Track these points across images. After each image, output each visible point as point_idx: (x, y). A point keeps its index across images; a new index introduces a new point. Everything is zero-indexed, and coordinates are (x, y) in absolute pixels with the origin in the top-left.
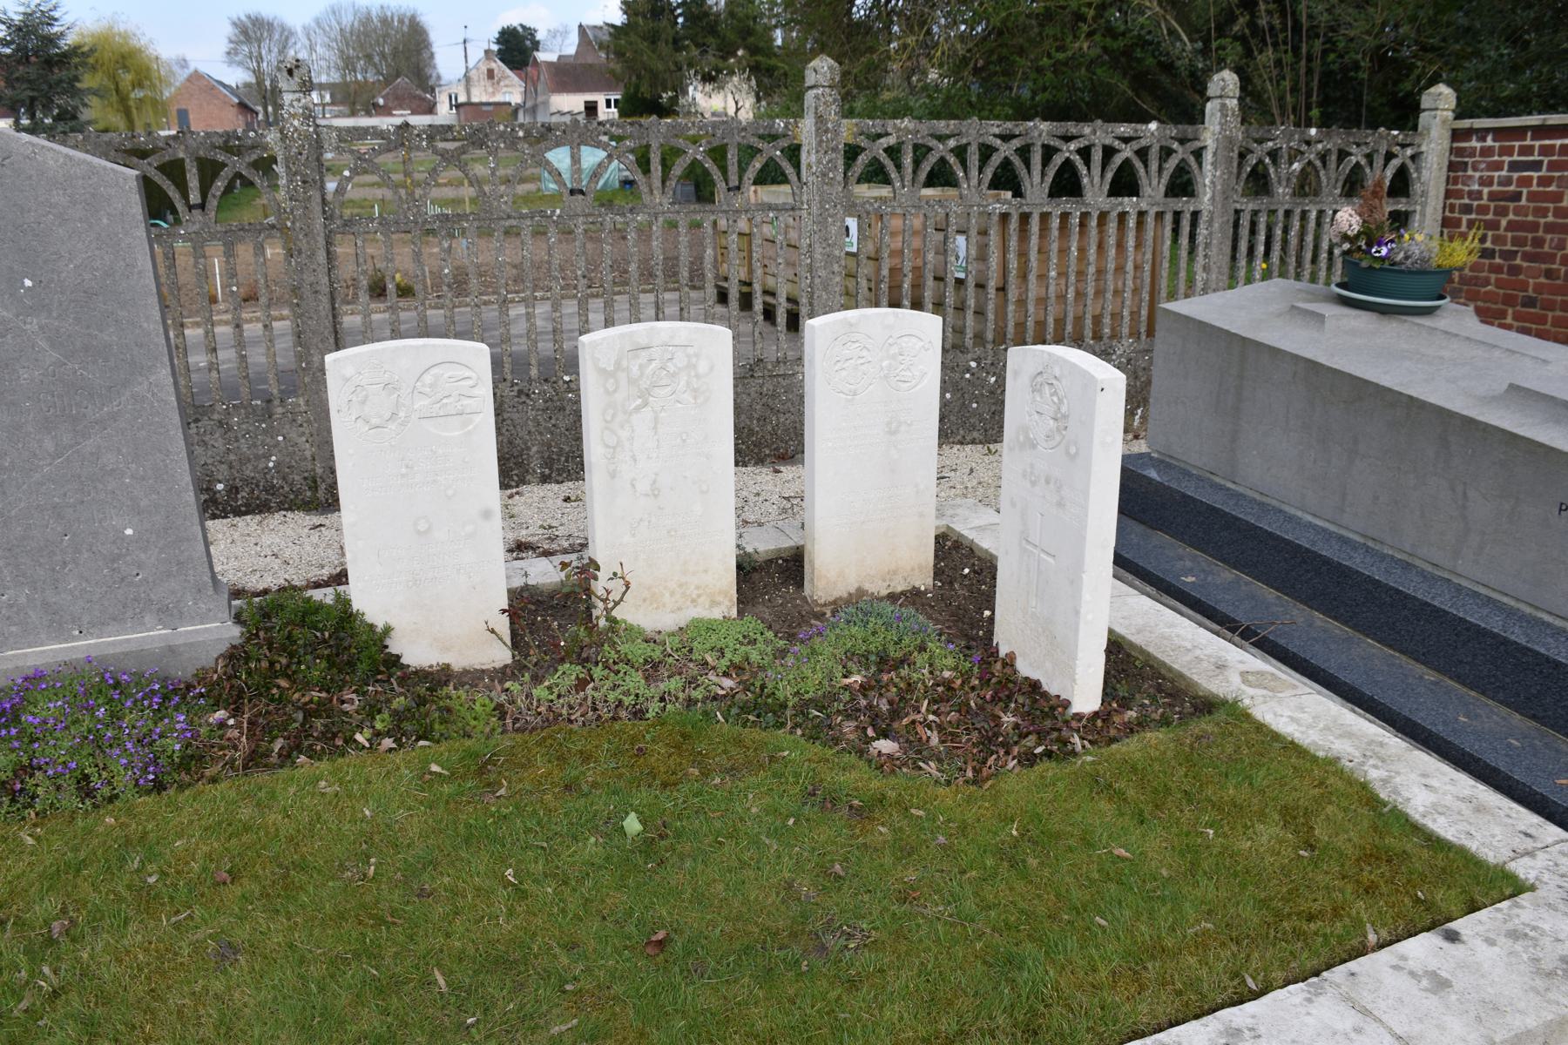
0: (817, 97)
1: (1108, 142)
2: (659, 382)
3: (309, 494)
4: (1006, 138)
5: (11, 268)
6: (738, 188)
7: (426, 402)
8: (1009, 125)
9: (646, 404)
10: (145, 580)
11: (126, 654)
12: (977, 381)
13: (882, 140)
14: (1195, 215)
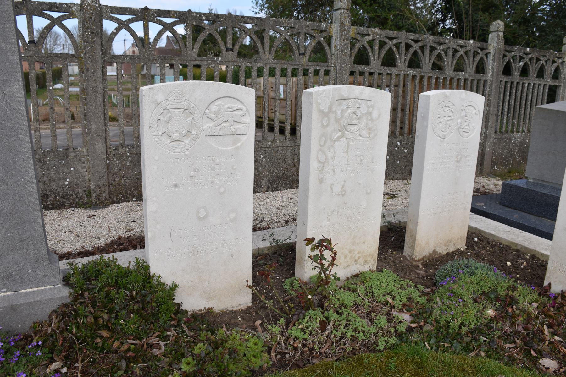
0: (341, 13)
1: (455, 47)
2: (346, 120)
3: (86, 199)
4: (416, 41)
6: (304, 54)
7: (212, 124)
8: (417, 36)
9: (343, 135)
12: (400, 152)
13: (367, 37)
14: (485, 81)
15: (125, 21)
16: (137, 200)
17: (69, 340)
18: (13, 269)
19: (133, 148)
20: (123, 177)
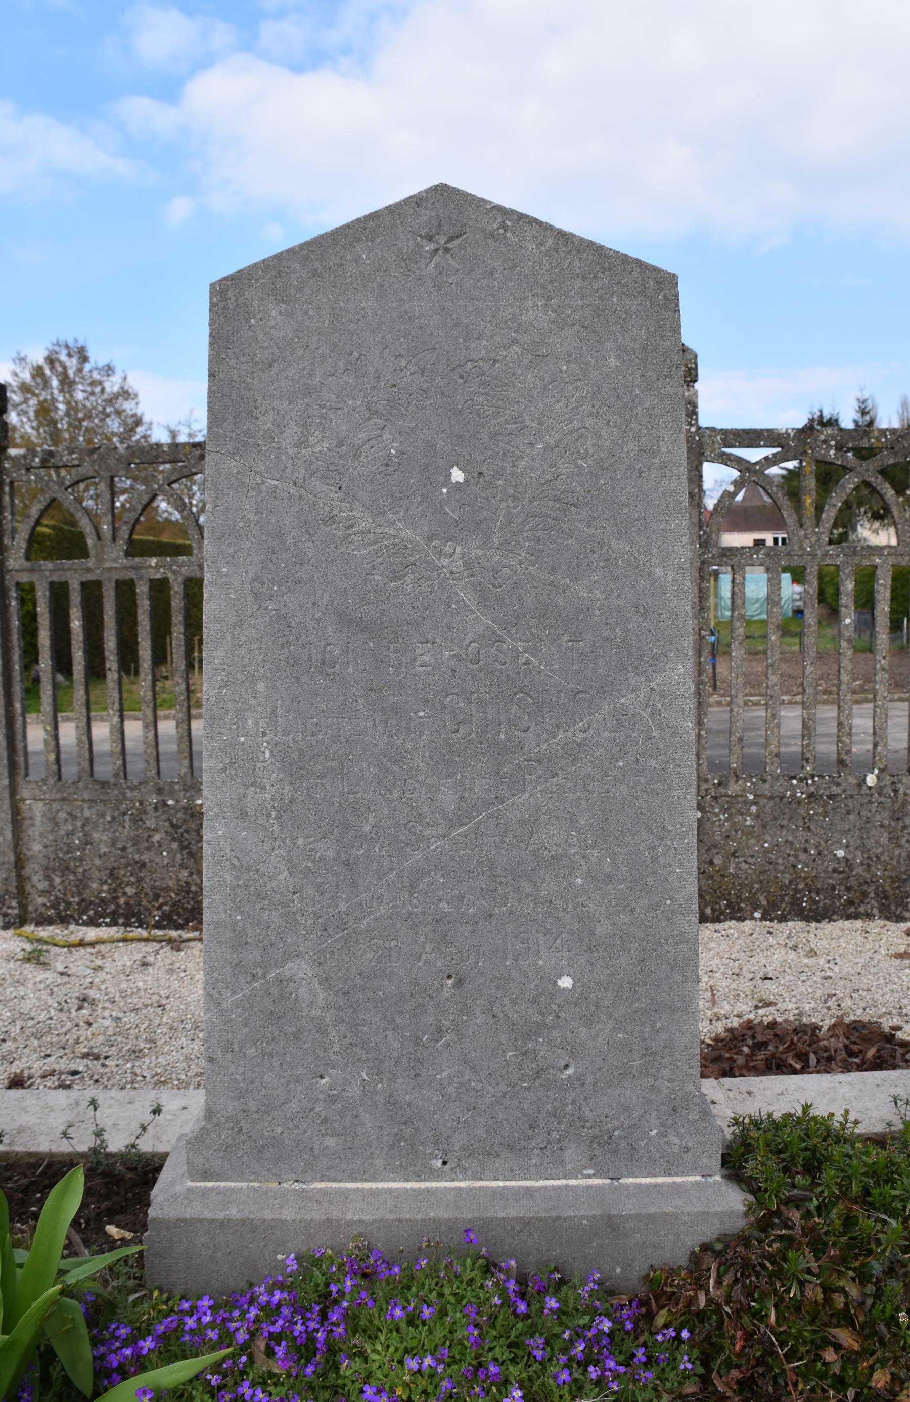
5: (431, 446)
10: (579, 1078)
11: (527, 1223)
15: (756, 463)
16: (763, 918)
17: (760, 1342)
18: (617, 1124)
19: (765, 781)
20: (733, 855)
